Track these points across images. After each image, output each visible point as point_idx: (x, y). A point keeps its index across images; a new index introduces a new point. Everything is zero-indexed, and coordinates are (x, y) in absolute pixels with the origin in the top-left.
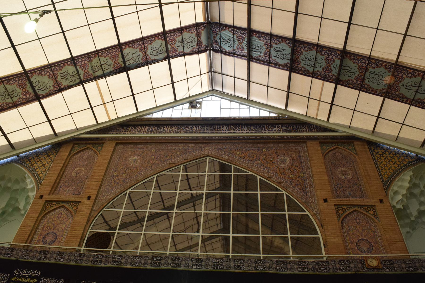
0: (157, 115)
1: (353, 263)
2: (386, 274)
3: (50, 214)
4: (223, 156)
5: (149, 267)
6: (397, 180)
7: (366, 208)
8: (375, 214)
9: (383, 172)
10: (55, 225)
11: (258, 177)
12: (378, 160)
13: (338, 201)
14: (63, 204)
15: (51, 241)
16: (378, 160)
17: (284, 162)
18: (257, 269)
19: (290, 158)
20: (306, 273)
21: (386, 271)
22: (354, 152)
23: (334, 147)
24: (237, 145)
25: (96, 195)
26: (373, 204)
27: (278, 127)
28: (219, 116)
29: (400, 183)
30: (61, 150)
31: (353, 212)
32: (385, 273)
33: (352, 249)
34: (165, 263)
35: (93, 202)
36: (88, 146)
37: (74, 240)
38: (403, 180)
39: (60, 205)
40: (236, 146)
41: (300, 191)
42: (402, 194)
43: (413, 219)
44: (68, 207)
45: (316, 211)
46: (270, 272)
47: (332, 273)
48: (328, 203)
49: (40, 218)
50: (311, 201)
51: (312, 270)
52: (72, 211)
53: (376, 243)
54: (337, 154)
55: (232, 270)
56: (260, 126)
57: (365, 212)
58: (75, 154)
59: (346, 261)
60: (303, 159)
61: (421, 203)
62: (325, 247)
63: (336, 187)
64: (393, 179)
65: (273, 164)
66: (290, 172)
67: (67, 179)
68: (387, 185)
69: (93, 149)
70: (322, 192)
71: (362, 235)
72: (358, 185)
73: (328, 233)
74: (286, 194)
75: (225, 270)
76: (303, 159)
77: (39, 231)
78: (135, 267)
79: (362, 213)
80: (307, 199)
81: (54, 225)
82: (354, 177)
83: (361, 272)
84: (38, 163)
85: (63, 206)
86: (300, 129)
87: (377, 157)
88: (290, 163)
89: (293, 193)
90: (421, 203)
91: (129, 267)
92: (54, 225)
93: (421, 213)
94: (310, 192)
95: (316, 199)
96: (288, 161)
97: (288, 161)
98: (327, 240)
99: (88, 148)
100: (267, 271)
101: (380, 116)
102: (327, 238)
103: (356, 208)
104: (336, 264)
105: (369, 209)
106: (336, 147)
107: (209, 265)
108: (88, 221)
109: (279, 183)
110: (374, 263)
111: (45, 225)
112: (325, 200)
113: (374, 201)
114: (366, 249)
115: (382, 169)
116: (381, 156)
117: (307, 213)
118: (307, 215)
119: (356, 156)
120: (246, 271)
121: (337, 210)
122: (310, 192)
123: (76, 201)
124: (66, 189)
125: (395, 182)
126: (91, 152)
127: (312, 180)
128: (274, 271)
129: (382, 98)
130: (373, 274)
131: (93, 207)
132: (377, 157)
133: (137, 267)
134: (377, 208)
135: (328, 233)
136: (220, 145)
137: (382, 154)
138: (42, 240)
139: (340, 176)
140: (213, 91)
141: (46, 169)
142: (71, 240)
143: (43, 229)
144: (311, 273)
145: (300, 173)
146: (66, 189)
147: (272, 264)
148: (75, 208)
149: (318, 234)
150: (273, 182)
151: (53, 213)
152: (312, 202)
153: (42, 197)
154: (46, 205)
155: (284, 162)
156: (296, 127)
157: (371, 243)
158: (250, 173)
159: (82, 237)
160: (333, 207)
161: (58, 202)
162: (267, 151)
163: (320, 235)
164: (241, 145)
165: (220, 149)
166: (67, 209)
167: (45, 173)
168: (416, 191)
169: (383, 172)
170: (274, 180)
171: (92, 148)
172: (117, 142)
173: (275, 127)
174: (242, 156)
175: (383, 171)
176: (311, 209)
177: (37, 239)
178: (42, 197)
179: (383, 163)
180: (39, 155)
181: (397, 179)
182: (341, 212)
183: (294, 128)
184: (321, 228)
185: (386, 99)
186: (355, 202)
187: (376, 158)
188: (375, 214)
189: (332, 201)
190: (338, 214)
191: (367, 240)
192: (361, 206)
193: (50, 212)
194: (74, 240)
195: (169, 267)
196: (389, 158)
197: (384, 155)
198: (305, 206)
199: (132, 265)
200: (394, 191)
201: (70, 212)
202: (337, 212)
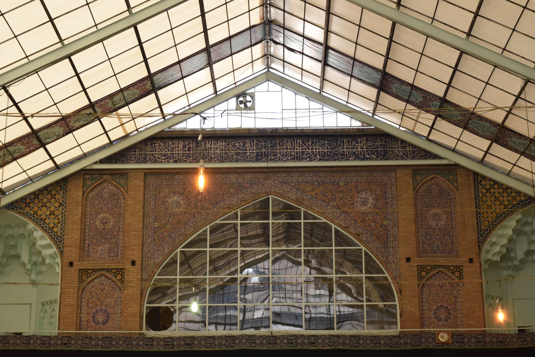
0: (193, 124)
1: (424, 337)
2: (454, 349)
4: (290, 195)
5: (224, 348)
6: (497, 229)
7: (453, 268)
8: (461, 277)
9: (483, 217)
10: (102, 299)
11: (334, 226)
12: (482, 197)
13: (423, 261)
14: (102, 272)
15: (103, 321)
16: (482, 197)
17: (364, 203)
18: (331, 346)
19: (373, 196)
20: (378, 349)
21: (455, 346)
22: (455, 185)
23: (430, 177)
24: (306, 175)
25: (141, 259)
26: (461, 265)
27: (361, 143)
28: (281, 127)
29: (501, 232)
30: (69, 186)
31: (437, 273)
32: (454, 348)
33: (429, 317)
34: (240, 342)
35: (140, 269)
37: (133, 319)
38: (506, 227)
39: (98, 274)
40: (306, 177)
41: (380, 246)
42: (501, 244)
43: (516, 263)
45: (396, 274)
46: (343, 348)
47: (402, 348)
48: (411, 264)
49: (80, 293)
50: (392, 261)
51: (384, 346)
52: (116, 281)
53: (455, 310)
54: (433, 186)
55: (306, 347)
56: (337, 140)
57: (450, 274)
58: (90, 192)
59: (419, 335)
60: (389, 198)
61: (531, 242)
62: (400, 317)
63: (424, 238)
64: (493, 227)
65: (352, 206)
66: (371, 218)
67: (93, 234)
68: (483, 236)
70: (405, 248)
71: (442, 302)
72: (451, 235)
73: (406, 302)
74: (365, 251)
75: (300, 347)
76: (389, 198)
77: (85, 309)
78: (210, 349)
79: (446, 275)
80: (387, 257)
81: (99, 300)
82: (448, 224)
83: (431, 347)
84: (43, 209)
85: (102, 275)
86: (390, 146)
87: (482, 193)
88: (372, 204)
89: (373, 249)
90: (531, 242)
91: (203, 349)
92: (99, 300)
93: (529, 253)
94: (393, 247)
95: (398, 257)
96: (371, 201)
97: (371, 201)
98: (404, 309)
100: (341, 347)
101: (489, 152)
102: (404, 307)
103: (442, 269)
104: (407, 339)
105: (455, 270)
106: (433, 176)
107: (283, 343)
108: (142, 294)
109: (357, 235)
110: (443, 338)
111: (88, 300)
112: (408, 260)
113: (462, 260)
114: (443, 317)
115: (483, 213)
116: (487, 192)
117: (387, 275)
118: (386, 278)
119: (456, 191)
120: (320, 348)
121: (420, 271)
122: (393, 247)
124: (96, 248)
125: (495, 232)
127: (396, 230)
128: (348, 347)
129: (489, 142)
130: (442, 349)
131: (142, 275)
132: (482, 193)
133: (212, 349)
134: (464, 269)
135: (406, 302)
136: (284, 175)
137: (490, 189)
138: (92, 320)
139: (431, 223)
140: (269, 76)
141: (58, 219)
142: (129, 319)
143: (88, 306)
144: (382, 348)
145: (384, 220)
147: (346, 339)
148: (119, 277)
149: (395, 301)
150: (351, 233)
151: (93, 284)
152: (393, 262)
153: (71, 264)
154: (81, 275)
155: (364, 203)
156: (386, 142)
157: (449, 310)
158: (324, 220)
159: (140, 315)
160: (416, 269)
161: (95, 270)
162: (345, 185)
163: (397, 303)
164: (311, 174)
165: (285, 183)
167: (59, 225)
168: (527, 229)
169: (483, 217)
170: (352, 231)
173: (357, 143)
174: (313, 193)
175: (484, 215)
176: (392, 270)
177: (86, 319)
178: (71, 264)
179: (487, 203)
180: (39, 195)
181: (499, 227)
182: (423, 274)
183: (383, 143)
184: (399, 295)
185: (494, 144)
186: (441, 261)
187: (481, 195)
188: (461, 277)
189: (416, 262)
190: (420, 277)
191: (446, 307)
192: (447, 267)
194: (133, 319)
195: (244, 347)
196: (497, 195)
197: (492, 190)
198: (385, 266)
199: (207, 347)
200: (492, 243)
202: (419, 274)
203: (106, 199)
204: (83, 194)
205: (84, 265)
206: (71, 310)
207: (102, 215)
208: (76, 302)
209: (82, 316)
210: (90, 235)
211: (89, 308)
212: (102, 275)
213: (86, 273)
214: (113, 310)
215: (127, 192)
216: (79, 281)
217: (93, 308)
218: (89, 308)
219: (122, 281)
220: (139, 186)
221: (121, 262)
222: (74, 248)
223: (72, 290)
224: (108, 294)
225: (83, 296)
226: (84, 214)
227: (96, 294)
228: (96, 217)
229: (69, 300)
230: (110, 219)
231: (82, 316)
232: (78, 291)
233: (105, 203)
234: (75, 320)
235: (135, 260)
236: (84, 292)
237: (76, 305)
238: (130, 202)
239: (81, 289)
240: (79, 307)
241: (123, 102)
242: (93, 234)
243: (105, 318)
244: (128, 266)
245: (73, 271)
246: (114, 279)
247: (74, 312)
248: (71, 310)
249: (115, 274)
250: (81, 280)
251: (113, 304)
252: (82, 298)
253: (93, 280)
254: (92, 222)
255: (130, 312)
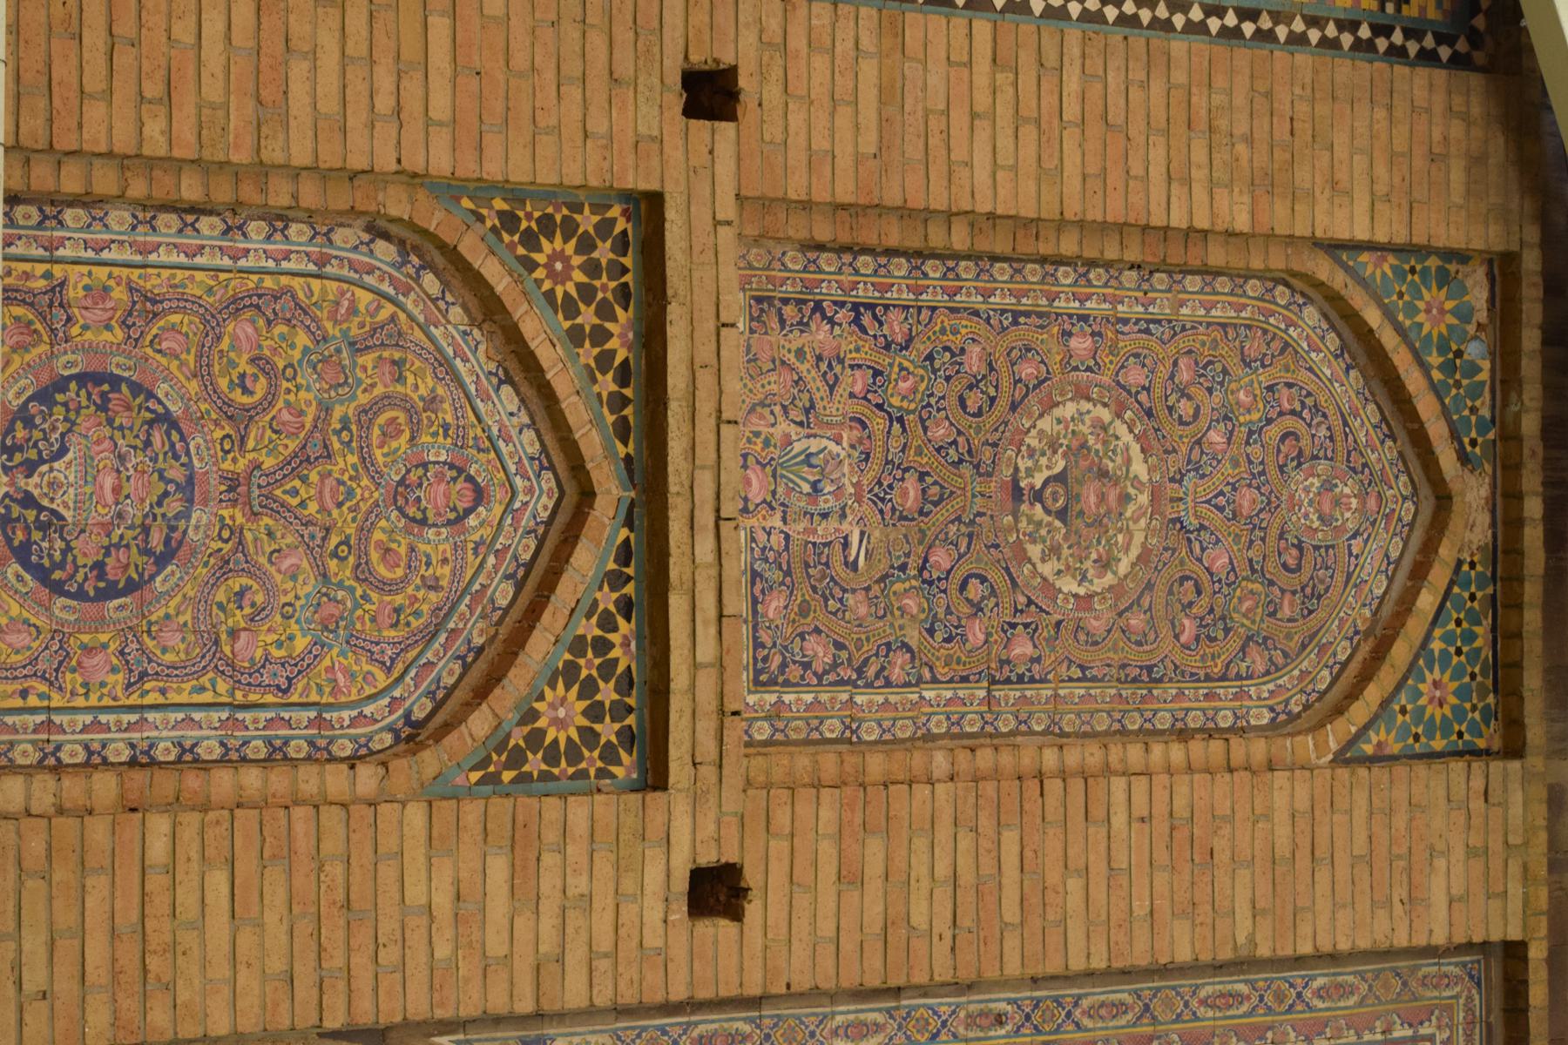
3: (453, 327)
10: (307, 494)
14: (611, 491)
15: (52, 522)
30: (1420, 84)
36: (1473, 493)
39: (593, 441)
44: (566, 592)
49: (396, 204)
67: (974, 362)
69: (1427, 601)
81: (299, 462)
85: (580, 495)
92: (299, 462)
99: (1443, 499)
123: (659, 693)
126: (1375, 559)
138: (68, 363)
142: (98, 886)
143: (235, 306)
146: (836, 407)
148: (562, 714)
151: (477, 362)
153: (710, 94)
154: (587, 221)
166: (539, 583)
171: (1439, 575)
172: (1537, 952)
188: (535, 763)
193: (490, 311)
201: (489, 671)
203: (1271, 506)
204: (1334, 248)
205: (708, 270)
206: (213, 91)
207: (1139, 468)
208: (301, 155)
209: (119, 218)
210: (966, 325)
211: (212, 323)
212: (580, 495)
213: (606, 286)
214: (174, 648)
215: (1343, 759)
216: (516, 195)
217: (202, 372)
218: (212, 323)
219: (519, 765)
220: (1412, 901)
221: (735, 730)
222: (869, 143)
223: (440, 106)
224: (363, 573)
225: (346, 237)
226: (1171, 253)
227: (367, 414)
228: (1122, 398)
229: (329, 61)
230: (1105, 564)
231: (119, 218)
232: (414, 179)
233: (1247, 499)
234: (94, 137)
235: (752, 910)
236: (385, 251)
237: (273, 153)
238: (1280, 801)
239: (435, 219)
240: (233, 195)
241: (944, 118)
242: (974, 362)
243: (87, 549)
244: (688, 831)
245: (648, 121)
246: (541, 647)
247: (185, 130)
248: (213, 91)
249: (588, 665)
250: (528, 218)
251: (249, 649)
252: (322, 222)
253: (522, 366)
254: (1080, 344)
255: (187, 900)
